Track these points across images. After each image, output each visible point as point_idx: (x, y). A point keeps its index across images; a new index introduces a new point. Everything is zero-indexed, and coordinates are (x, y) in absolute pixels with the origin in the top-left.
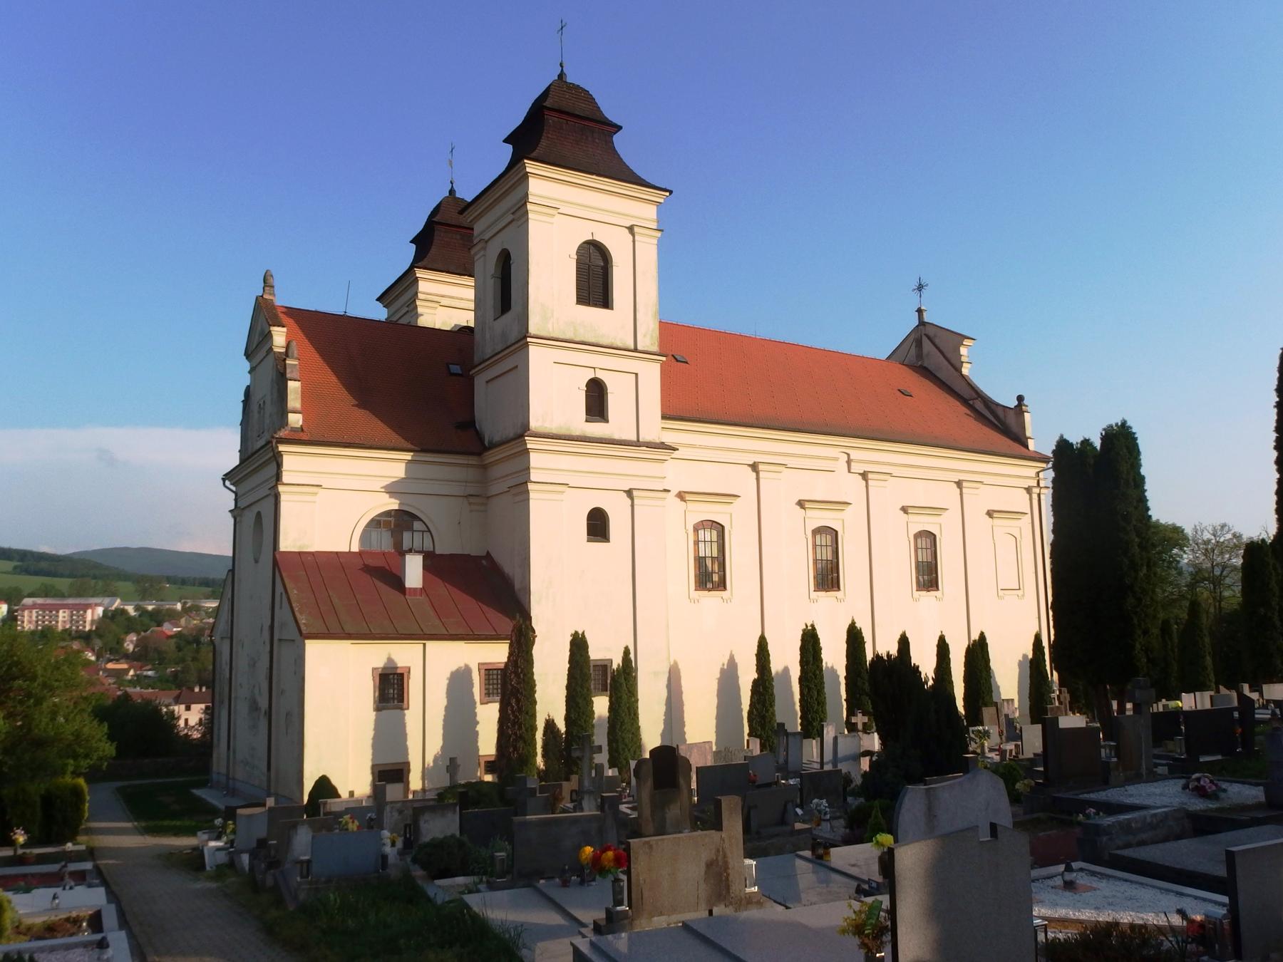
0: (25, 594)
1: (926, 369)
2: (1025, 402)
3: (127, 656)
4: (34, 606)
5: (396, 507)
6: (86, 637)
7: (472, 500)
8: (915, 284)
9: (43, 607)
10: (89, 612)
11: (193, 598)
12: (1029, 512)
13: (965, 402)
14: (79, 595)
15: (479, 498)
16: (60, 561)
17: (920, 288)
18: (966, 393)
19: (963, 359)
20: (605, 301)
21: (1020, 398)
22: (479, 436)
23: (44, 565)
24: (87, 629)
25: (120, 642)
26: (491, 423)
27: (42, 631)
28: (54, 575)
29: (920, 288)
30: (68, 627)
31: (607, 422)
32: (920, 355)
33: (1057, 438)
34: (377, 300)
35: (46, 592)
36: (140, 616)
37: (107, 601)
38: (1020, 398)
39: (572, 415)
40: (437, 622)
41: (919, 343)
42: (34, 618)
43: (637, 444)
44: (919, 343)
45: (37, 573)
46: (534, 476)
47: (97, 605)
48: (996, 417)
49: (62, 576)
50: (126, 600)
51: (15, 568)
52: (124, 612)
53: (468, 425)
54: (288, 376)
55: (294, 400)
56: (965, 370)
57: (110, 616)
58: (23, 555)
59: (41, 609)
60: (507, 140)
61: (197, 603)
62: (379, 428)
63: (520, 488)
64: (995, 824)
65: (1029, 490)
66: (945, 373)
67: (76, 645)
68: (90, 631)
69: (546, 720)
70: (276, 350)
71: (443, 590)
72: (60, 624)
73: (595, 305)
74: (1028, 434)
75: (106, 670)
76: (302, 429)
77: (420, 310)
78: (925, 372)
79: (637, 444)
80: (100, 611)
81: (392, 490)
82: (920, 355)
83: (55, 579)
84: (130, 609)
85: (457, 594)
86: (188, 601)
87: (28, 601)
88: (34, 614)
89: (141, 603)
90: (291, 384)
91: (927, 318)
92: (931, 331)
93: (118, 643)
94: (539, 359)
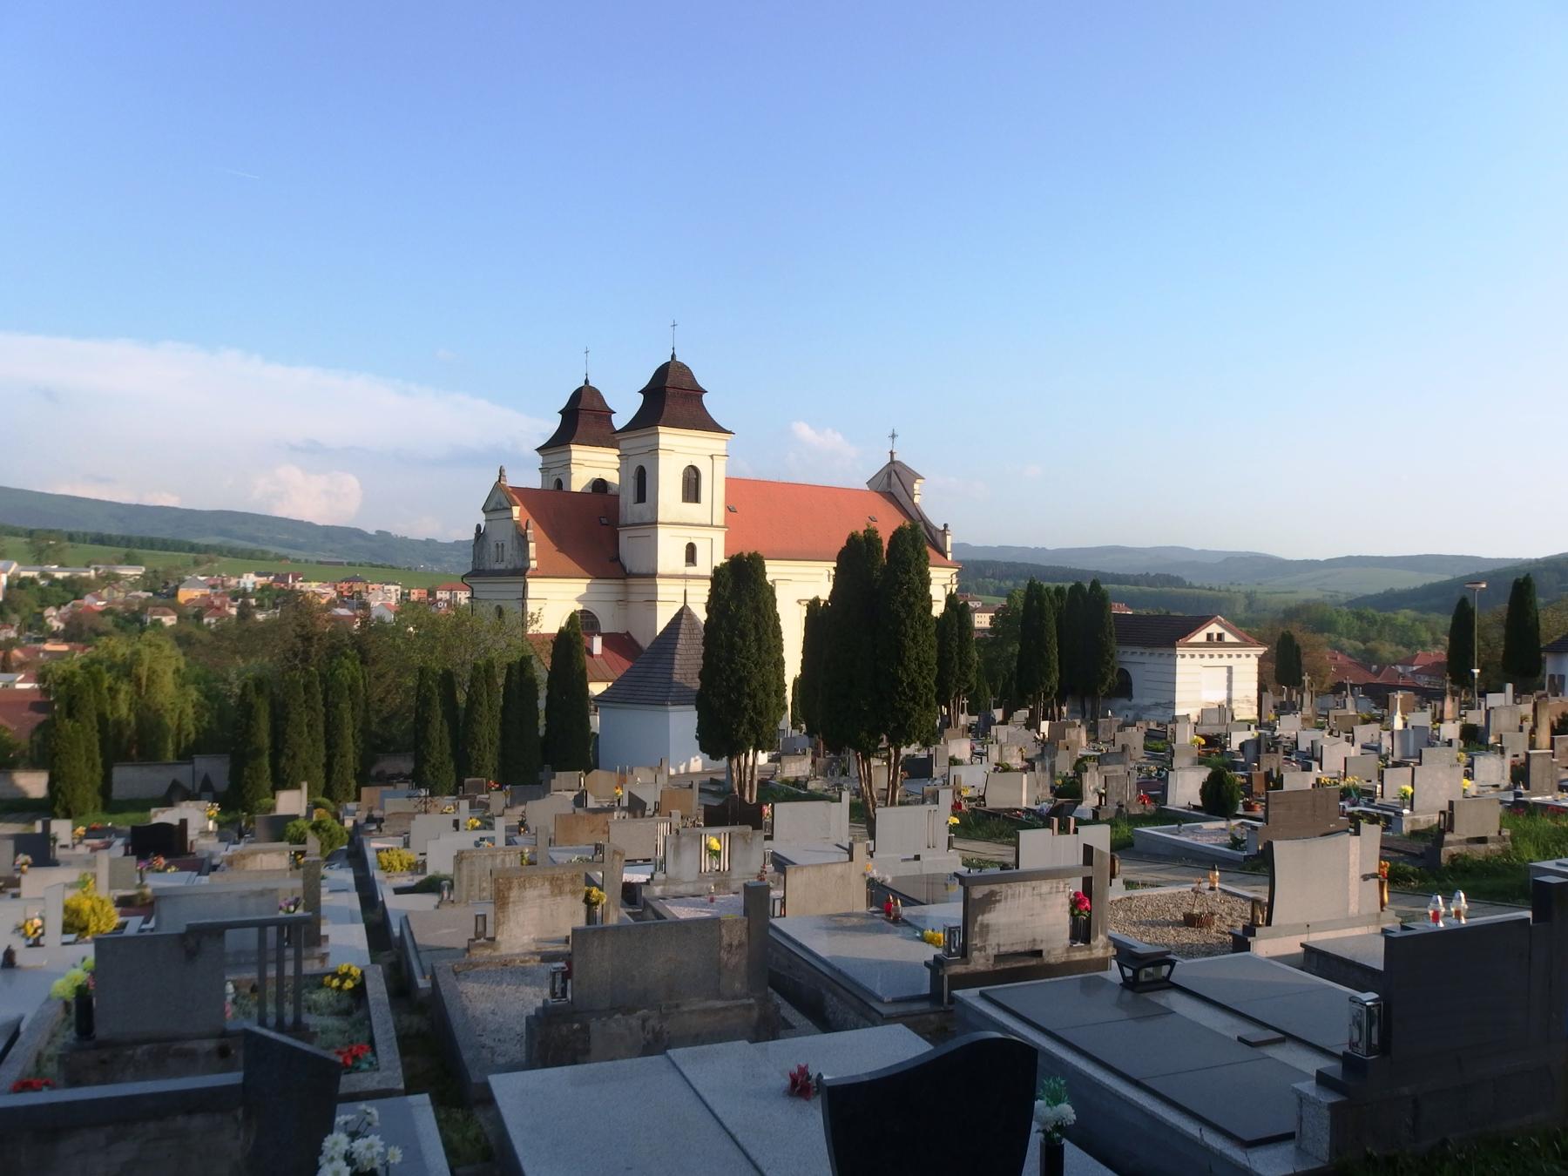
1: (892, 494)
2: (949, 528)
3: (55, 635)
5: (581, 608)
7: (620, 603)
11: (108, 564)
15: (624, 602)
17: (893, 436)
19: (915, 492)
20: (697, 499)
21: (946, 526)
22: (624, 568)
26: (631, 559)
29: (893, 436)
31: (696, 565)
32: (889, 485)
34: (538, 450)
38: (946, 526)
40: (612, 672)
41: (890, 477)
43: (712, 525)
48: (930, 533)
54: (529, 539)
55: (532, 554)
56: (916, 500)
61: (111, 570)
62: (574, 567)
64: (1092, 848)
65: (945, 586)
66: (904, 499)
70: (515, 519)
71: (611, 655)
73: (692, 502)
76: (537, 569)
77: (573, 470)
78: (891, 497)
81: (579, 600)
82: (889, 485)
85: (617, 656)
86: (100, 566)
91: (896, 458)
92: (897, 468)
94: (663, 533)
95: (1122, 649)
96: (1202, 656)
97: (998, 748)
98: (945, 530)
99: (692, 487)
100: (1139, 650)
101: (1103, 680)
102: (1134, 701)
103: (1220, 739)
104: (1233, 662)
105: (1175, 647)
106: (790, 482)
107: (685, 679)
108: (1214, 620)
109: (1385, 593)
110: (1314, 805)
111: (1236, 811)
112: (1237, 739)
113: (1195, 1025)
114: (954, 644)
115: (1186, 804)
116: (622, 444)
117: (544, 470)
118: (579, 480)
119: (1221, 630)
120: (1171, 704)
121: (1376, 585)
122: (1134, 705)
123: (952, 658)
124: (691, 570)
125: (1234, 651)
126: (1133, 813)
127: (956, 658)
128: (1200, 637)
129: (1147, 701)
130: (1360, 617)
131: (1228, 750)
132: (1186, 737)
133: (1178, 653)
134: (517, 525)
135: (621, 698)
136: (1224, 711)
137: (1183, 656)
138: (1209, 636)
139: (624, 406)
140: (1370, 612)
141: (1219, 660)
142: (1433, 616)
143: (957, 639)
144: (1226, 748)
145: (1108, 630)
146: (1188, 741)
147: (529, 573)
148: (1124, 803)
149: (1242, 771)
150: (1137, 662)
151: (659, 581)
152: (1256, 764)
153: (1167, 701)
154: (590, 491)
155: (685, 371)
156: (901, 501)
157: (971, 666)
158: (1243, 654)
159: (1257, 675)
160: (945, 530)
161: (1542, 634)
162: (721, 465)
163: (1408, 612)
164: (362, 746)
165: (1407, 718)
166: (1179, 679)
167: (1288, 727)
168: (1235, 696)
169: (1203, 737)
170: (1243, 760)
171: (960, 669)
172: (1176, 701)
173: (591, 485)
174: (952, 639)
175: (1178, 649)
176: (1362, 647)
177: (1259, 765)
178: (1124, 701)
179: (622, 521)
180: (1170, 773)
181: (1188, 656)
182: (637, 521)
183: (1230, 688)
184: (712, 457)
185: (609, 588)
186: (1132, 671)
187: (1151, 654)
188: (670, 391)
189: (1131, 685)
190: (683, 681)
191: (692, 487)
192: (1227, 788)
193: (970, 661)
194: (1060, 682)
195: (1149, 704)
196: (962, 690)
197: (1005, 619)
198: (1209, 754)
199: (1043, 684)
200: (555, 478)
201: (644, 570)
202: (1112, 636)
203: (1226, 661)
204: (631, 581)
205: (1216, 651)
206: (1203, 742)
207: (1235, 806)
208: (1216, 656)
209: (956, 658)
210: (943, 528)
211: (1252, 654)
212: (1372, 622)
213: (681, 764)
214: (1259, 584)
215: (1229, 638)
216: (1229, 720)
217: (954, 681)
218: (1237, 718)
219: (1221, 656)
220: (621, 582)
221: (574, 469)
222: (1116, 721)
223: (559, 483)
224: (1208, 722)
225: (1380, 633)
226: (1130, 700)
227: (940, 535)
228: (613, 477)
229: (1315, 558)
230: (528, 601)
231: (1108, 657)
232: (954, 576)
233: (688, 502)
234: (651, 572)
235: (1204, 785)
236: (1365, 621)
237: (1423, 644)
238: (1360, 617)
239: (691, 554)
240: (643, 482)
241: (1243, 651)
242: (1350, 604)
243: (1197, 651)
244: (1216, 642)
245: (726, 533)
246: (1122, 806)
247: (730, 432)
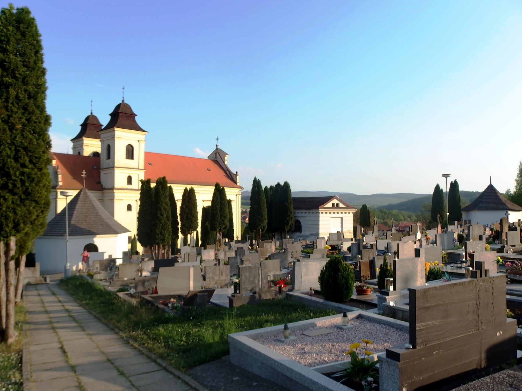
2: (238, 173)
8: (216, 138)
12: (236, 200)
13: (225, 171)
17: (217, 139)
18: (226, 169)
19: (225, 160)
21: (237, 172)
22: (102, 186)
26: (105, 183)
29: (217, 139)
32: (216, 157)
33: (202, 207)
38: (237, 172)
39: (125, 185)
41: (216, 154)
43: (139, 169)
44: (216, 154)
48: (231, 176)
53: (99, 182)
56: (226, 163)
60: (110, 115)
63: (112, 199)
65: (236, 195)
66: (221, 163)
69: (321, 270)
73: (130, 159)
74: (238, 181)
78: (216, 162)
82: (216, 157)
91: (219, 147)
92: (219, 151)
94: (117, 172)
95: (297, 211)
96: (330, 213)
97: (224, 253)
98: (236, 174)
99: (130, 153)
100: (304, 211)
101: (288, 223)
102: (303, 233)
103: (338, 247)
104: (343, 215)
105: (318, 209)
106: (180, 155)
107: (78, 223)
108: (335, 197)
109: (389, 205)
110: (478, 306)
111: (350, 296)
112: (346, 246)
114: (218, 207)
115: (308, 290)
116: (102, 136)
117: (74, 148)
118: (87, 151)
119: (338, 202)
120: (318, 234)
121: (385, 203)
122: (302, 235)
123: (217, 213)
124: (130, 187)
125: (344, 211)
126: (265, 298)
127: (219, 213)
128: (329, 205)
129: (308, 233)
130: (381, 212)
131: (342, 251)
132: (322, 246)
133: (320, 211)
134: (54, 167)
135: (55, 233)
136: (340, 235)
137: (322, 213)
138: (333, 204)
139: (104, 120)
140: (385, 210)
141: (337, 215)
142: (403, 212)
143: (219, 204)
144: (341, 250)
145: (289, 201)
146: (323, 248)
147: (58, 187)
148: (257, 290)
149: (350, 261)
150: (303, 216)
151: (115, 191)
152: (360, 256)
153: (316, 233)
154: (92, 156)
155: (128, 107)
156: (220, 163)
157: (226, 217)
158: (347, 212)
159: (353, 221)
160: (236, 174)
161: (461, 204)
162: (143, 145)
163: (396, 210)
165: (427, 233)
166: (321, 223)
167: (369, 239)
168: (344, 230)
169: (331, 246)
170: (350, 255)
171: (221, 218)
172: (320, 232)
173: (92, 154)
174: (217, 205)
175: (320, 210)
176: (383, 221)
177: (362, 256)
178: (298, 234)
179: (101, 167)
180: (297, 263)
181: (324, 213)
182: (107, 167)
183: (342, 227)
186: (301, 220)
187: (309, 213)
188: (121, 114)
189: (301, 226)
190: (76, 224)
191: (130, 153)
192: (343, 275)
193: (225, 214)
194: (269, 224)
195: (308, 234)
196: (222, 228)
198: (333, 253)
199: (260, 225)
200: (78, 152)
201: (110, 187)
202: (291, 204)
203: (340, 215)
204: (105, 191)
205: (336, 211)
206: (330, 248)
207: (350, 293)
208: (336, 213)
209: (219, 213)
210: (235, 173)
211: (351, 212)
212: (385, 213)
213: (74, 266)
214: (350, 203)
215: (341, 205)
216: (342, 238)
217: (218, 223)
218: (345, 237)
219: (338, 213)
220: (100, 192)
221: (84, 147)
222: (291, 240)
223: (79, 153)
224: (333, 239)
225: (388, 217)
226: (301, 233)
227: (234, 176)
228: (99, 150)
229: (367, 194)
230: (58, 199)
231: (289, 213)
234: (112, 188)
235: (323, 273)
236: (383, 213)
237: (401, 220)
238: (381, 212)
239: (130, 180)
240: (109, 150)
241: (347, 211)
242: (378, 208)
243: (328, 211)
244: (336, 207)
245: (145, 172)
246: (255, 293)
247: (147, 132)
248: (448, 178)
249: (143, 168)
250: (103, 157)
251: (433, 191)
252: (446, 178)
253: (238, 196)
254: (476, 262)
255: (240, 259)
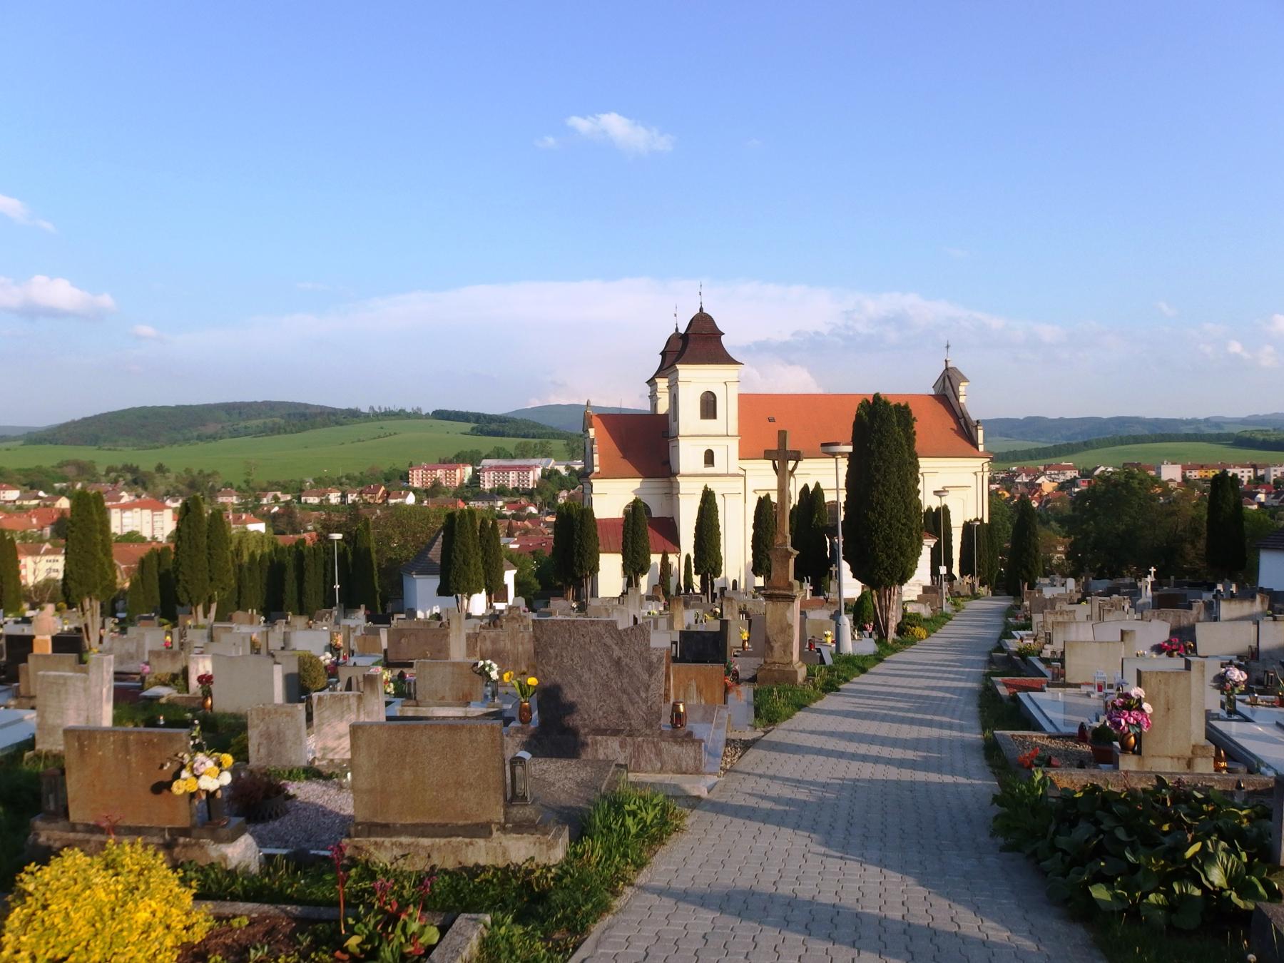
0: (483, 455)
4: (491, 468)
6: (529, 494)
9: (497, 468)
10: (531, 473)
14: (524, 456)
16: (505, 421)
19: (961, 393)
23: (494, 426)
24: (530, 487)
25: (555, 497)
27: (498, 489)
28: (502, 435)
29: (948, 347)
30: (516, 485)
35: (498, 454)
36: (569, 475)
37: (544, 461)
39: (700, 466)
41: (944, 380)
42: (492, 479)
43: (728, 436)
44: (944, 380)
45: (489, 434)
46: (681, 492)
47: (536, 467)
49: (508, 436)
50: (558, 460)
51: (473, 429)
52: (557, 472)
55: (596, 462)
56: (962, 400)
57: (549, 475)
58: (478, 418)
59: (496, 471)
65: (975, 473)
66: (953, 400)
67: (523, 501)
68: (533, 488)
72: (510, 483)
73: (710, 418)
75: (545, 522)
79: (727, 475)
80: (539, 471)
83: (505, 439)
84: (562, 470)
87: (486, 462)
88: (492, 475)
89: (570, 463)
90: (595, 455)
91: (950, 365)
93: (554, 498)
99: (709, 407)
113: (272, 683)
164: (624, 623)
184: (725, 383)
185: (655, 484)
191: (709, 407)
197: (1094, 491)
220: (665, 480)
232: (986, 465)
233: (707, 418)
248: (943, 498)
249: (736, 433)
250: (671, 418)
251: (601, 563)
252: (940, 497)
253: (980, 475)
254: (180, 733)
255: (85, 663)
